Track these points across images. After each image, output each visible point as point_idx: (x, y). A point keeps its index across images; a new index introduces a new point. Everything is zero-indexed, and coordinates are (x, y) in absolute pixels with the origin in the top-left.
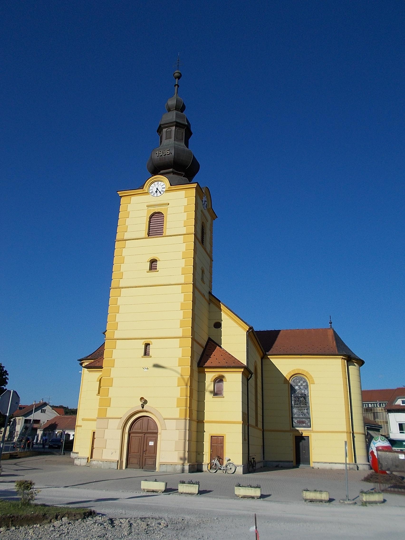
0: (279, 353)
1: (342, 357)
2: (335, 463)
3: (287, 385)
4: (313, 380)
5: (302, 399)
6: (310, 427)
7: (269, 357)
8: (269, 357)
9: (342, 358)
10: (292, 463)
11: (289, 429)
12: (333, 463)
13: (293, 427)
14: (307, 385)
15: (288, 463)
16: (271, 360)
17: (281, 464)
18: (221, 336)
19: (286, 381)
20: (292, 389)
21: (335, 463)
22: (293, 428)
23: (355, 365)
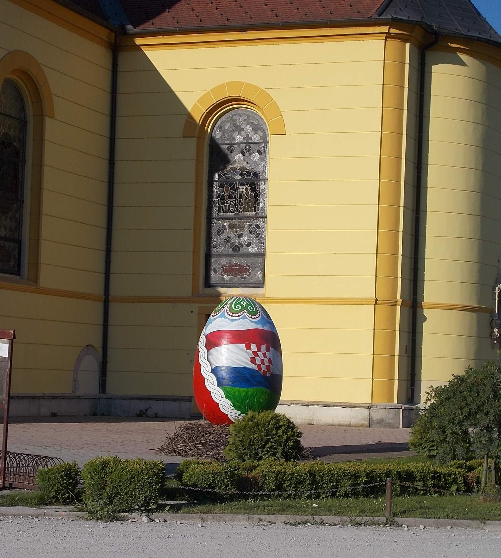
0: (177, 27)
1: (385, 29)
2: (326, 405)
3: (192, 143)
4: (282, 121)
5: (244, 190)
6: (261, 284)
7: (139, 41)
8: (139, 41)
9: (389, 36)
10: (188, 404)
11: (187, 291)
12: (318, 404)
13: (208, 283)
14: (265, 142)
15: (177, 404)
16: (152, 54)
17: (156, 407)
18: (453, 64)
19: (191, 128)
20: (218, 158)
21: (326, 405)
22: (209, 290)
23: (462, 63)
